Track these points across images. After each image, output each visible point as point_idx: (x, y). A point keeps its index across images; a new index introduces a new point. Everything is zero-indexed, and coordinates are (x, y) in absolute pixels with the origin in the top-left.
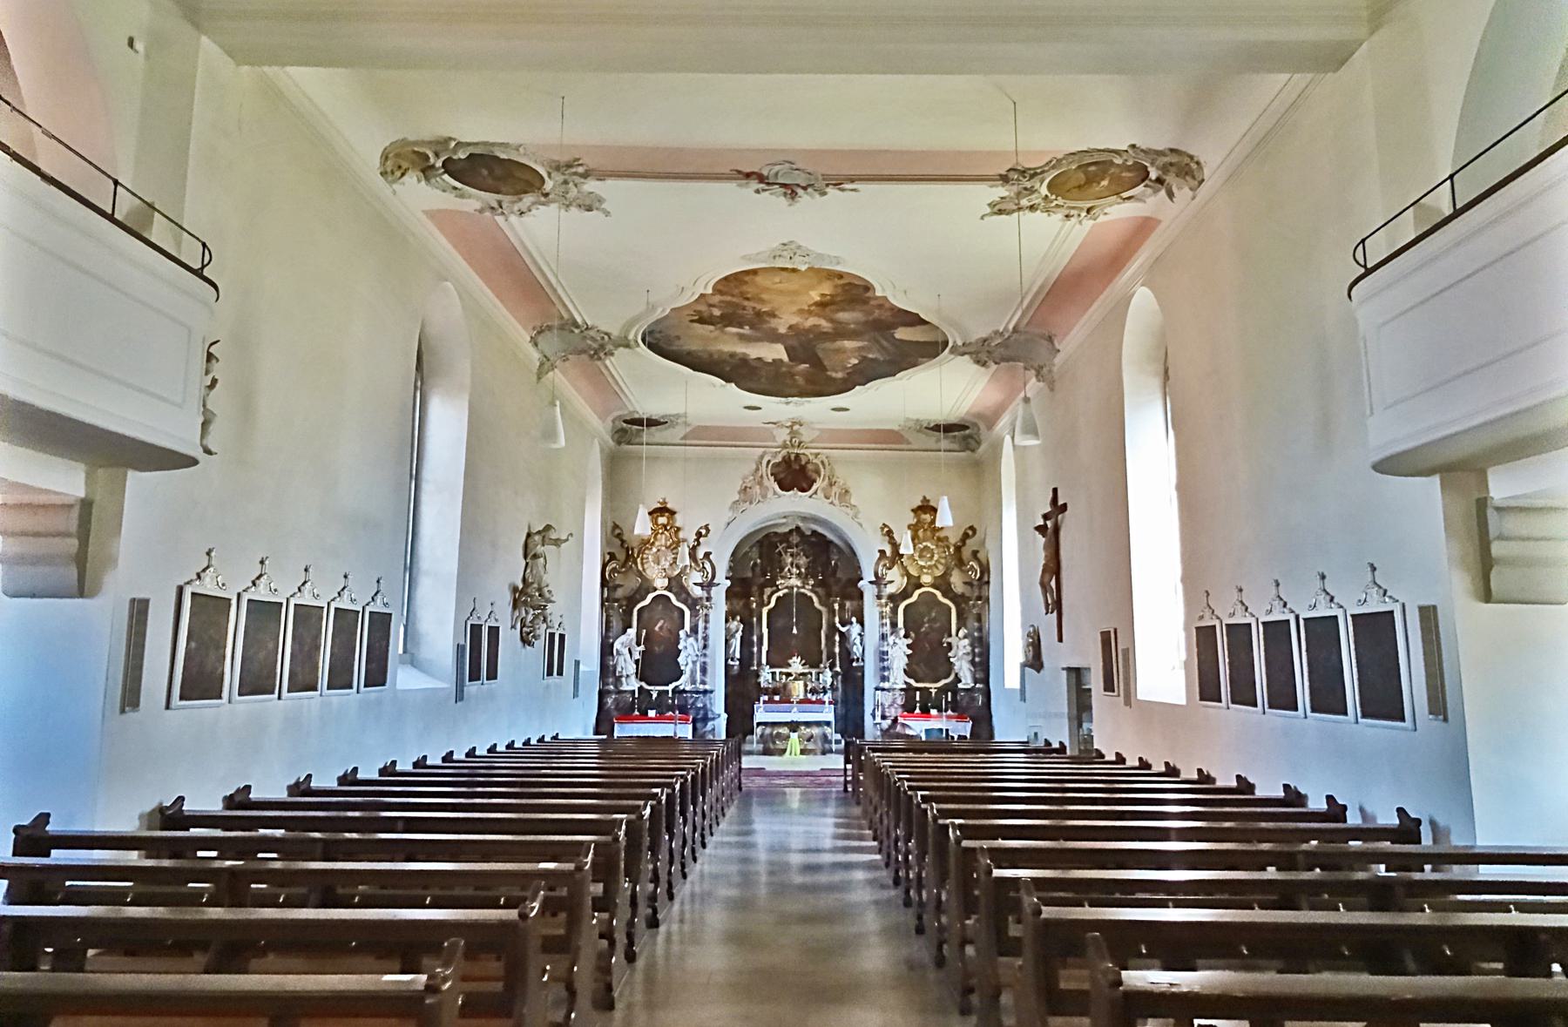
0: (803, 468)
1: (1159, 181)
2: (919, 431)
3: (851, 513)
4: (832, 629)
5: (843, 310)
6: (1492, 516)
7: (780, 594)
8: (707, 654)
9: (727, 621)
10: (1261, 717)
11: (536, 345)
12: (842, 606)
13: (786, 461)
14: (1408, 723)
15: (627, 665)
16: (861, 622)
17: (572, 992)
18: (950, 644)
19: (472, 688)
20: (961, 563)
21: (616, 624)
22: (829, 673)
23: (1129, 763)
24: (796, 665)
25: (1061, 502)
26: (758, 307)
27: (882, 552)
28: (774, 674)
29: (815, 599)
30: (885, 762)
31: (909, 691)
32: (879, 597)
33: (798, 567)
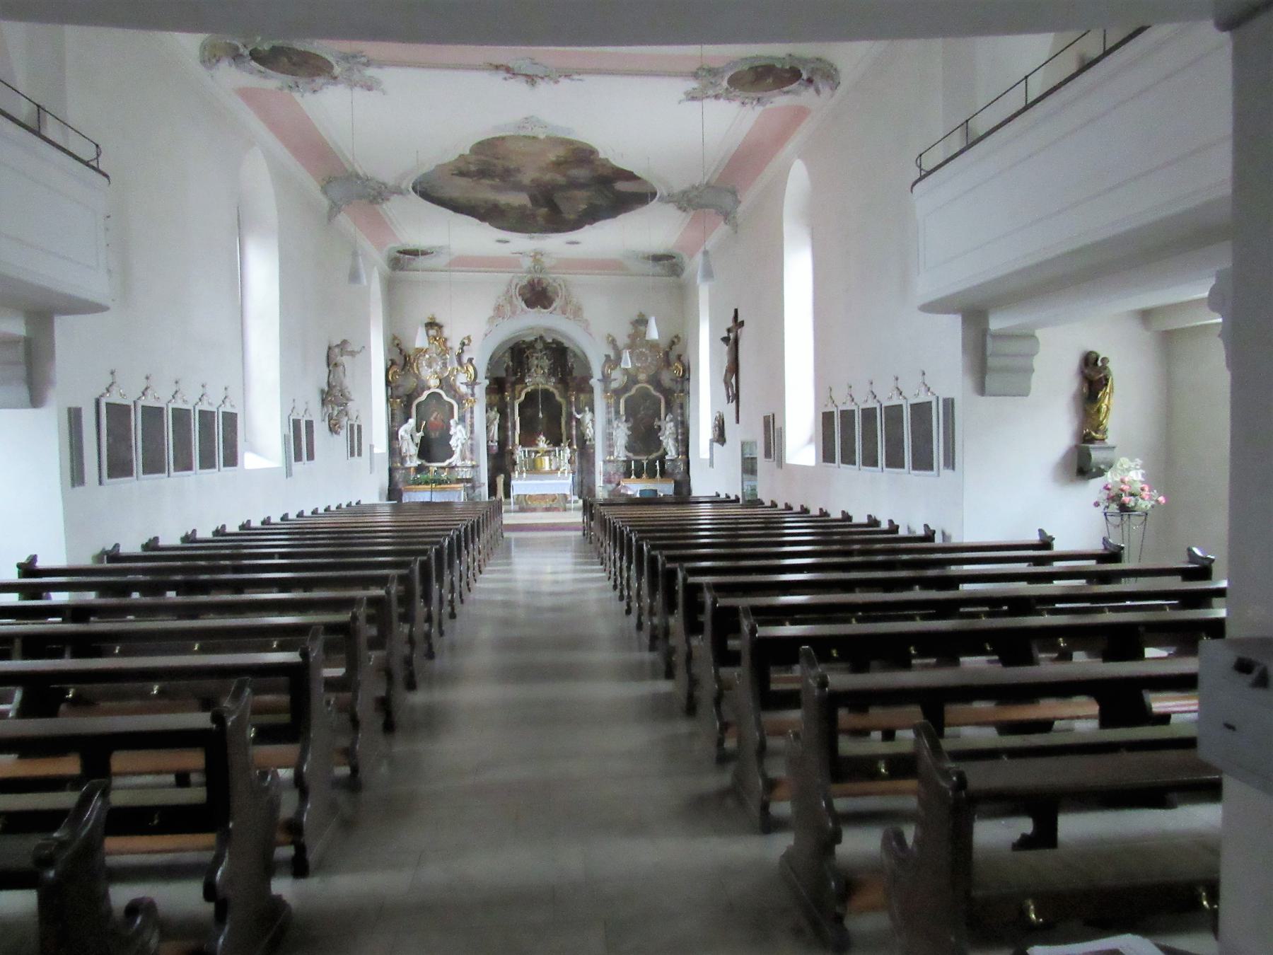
1: (810, 81)
6: (989, 340)
7: (529, 389)
10: (882, 475)
15: (410, 449)
16: (592, 410)
17: (355, 723)
19: (297, 467)
21: (399, 415)
22: (568, 451)
23: (812, 513)
24: (542, 443)
27: (608, 357)
30: (608, 513)
31: (628, 462)
32: (606, 391)
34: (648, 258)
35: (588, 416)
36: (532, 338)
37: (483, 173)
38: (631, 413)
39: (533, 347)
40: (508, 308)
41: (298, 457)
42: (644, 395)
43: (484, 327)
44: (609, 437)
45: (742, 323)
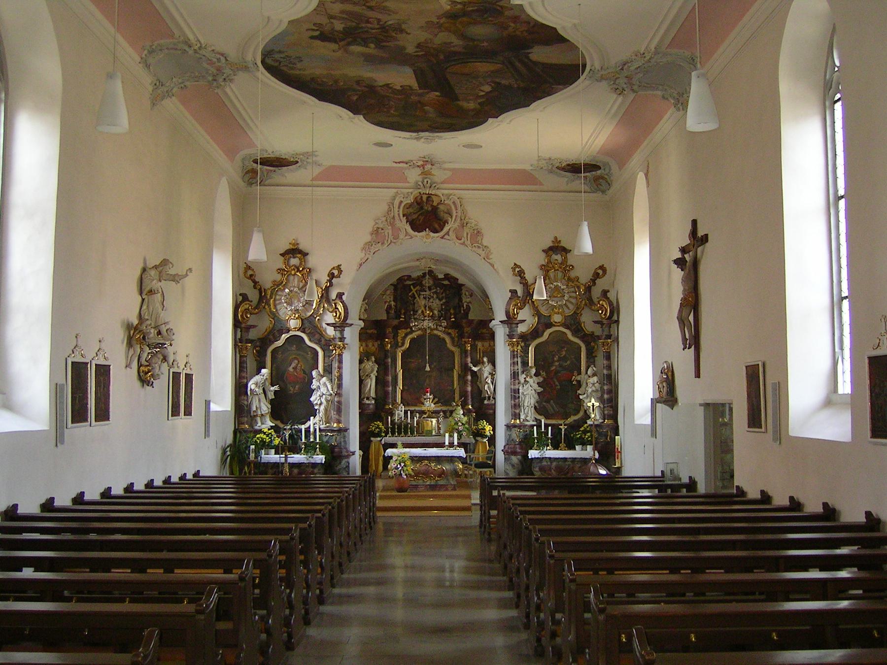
0: (435, 209)
2: (551, 172)
3: (483, 254)
4: (465, 369)
5: (475, 23)
7: (414, 335)
8: (337, 391)
9: (361, 362)
11: (148, 66)
12: (474, 347)
13: (419, 203)
14: (763, 430)
16: (493, 362)
18: (579, 382)
20: (591, 302)
21: (251, 364)
24: (429, 405)
25: (700, 233)
26: (384, 18)
27: (513, 292)
28: (406, 412)
29: (448, 340)
32: (510, 336)
33: (431, 310)
34: (563, 169)
35: (487, 369)
36: (420, 273)
37: (352, 35)
38: (542, 364)
39: (421, 285)
40: (389, 231)
41: (79, 415)
42: (560, 341)
43: (360, 255)
44: (515, 394)
45: (705, 239)
